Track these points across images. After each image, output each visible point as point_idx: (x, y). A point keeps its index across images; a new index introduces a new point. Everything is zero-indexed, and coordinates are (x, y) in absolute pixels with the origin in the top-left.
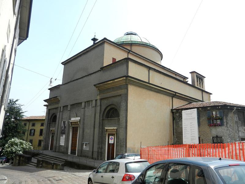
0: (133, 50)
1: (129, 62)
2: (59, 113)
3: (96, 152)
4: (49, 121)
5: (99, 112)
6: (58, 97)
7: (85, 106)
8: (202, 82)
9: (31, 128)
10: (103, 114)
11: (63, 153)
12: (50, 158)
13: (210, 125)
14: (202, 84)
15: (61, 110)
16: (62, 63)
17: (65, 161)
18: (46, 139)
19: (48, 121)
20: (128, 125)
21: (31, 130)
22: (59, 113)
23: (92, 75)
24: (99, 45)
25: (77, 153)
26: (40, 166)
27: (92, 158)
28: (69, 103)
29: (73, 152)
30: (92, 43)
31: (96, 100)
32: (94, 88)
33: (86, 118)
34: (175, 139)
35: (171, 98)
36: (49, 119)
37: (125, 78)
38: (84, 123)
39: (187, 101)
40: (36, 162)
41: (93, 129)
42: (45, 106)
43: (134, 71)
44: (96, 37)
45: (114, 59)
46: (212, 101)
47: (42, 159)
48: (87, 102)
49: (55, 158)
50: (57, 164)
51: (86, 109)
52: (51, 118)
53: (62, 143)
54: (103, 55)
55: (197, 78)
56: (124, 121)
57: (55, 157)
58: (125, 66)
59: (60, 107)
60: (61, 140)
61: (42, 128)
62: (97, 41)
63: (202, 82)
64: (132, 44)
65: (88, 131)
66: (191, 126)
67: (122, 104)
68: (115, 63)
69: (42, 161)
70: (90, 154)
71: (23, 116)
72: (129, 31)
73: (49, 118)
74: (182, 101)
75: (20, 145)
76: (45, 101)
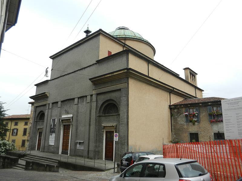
0: (128, 46)
1: (129, 54)
2: (47, 111)
3: (92, 151)
4: (36, 119)
5: (95, 108)
6: (46, 94)
7: (78, 102)
8: (195, 79)
9: (13, 127)
10: (100, 109)
11: (53, 153)
12: (40, 159)
13: (212, 122)
14: (195, 81)
15: (50, 107)
16: (51, 57)
17: (58, 161)
18: (32, 140)
19: (34, 119)
20: (129, 121)
21: (13, 130)
22: (47, 111)
23: (86, 69)
24: (91, 37)
25: (69, 153)
26: (30, 168)
27: (88, 158)
28: (59, 99)
29: (65, 151)
30: (84, 35)
31: (91, 95)
32: (90, 83)
33: (84, 113)
34: (174, 136)
35: (168, 94)
36: (36, 116)
37: (126, 71)
38: (77, 121)
39: (183, 97)
40: (25, 164)
41: (88, 127)
42: (29, 103)
43: (135, 64)
44: (90, 29)
45: (109, 52)
46: (204, 97)
47: (31, 161)
48: (81, 97)
49: (45, 159)
50: (51, 165)
51: (79, 105)
52: (38, 116)
53: (52, 142)
54: (99, 47)
55: (190, 75)
56: (126, 116)
57: (46, 158)
58: (125, 58)
59: (49, 104)
60: (50, 139)
61: (26, 127)
62: (91, 34)
63: (195, 79)
64: (126, 39)
65: (83, 129)
66: (237, 118)
67: (122, 99)
68: (111, 57)
69: (47, 165)
70: (85, 154)
71: (5, 114)
72: (121, 25)
73: (35, 115)
74: (179, 97)
75: (3, 146)
76: (31, 97)
